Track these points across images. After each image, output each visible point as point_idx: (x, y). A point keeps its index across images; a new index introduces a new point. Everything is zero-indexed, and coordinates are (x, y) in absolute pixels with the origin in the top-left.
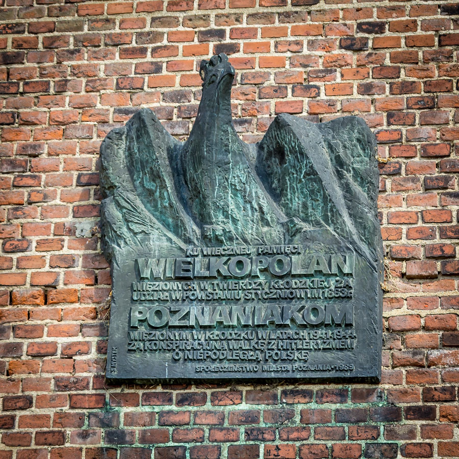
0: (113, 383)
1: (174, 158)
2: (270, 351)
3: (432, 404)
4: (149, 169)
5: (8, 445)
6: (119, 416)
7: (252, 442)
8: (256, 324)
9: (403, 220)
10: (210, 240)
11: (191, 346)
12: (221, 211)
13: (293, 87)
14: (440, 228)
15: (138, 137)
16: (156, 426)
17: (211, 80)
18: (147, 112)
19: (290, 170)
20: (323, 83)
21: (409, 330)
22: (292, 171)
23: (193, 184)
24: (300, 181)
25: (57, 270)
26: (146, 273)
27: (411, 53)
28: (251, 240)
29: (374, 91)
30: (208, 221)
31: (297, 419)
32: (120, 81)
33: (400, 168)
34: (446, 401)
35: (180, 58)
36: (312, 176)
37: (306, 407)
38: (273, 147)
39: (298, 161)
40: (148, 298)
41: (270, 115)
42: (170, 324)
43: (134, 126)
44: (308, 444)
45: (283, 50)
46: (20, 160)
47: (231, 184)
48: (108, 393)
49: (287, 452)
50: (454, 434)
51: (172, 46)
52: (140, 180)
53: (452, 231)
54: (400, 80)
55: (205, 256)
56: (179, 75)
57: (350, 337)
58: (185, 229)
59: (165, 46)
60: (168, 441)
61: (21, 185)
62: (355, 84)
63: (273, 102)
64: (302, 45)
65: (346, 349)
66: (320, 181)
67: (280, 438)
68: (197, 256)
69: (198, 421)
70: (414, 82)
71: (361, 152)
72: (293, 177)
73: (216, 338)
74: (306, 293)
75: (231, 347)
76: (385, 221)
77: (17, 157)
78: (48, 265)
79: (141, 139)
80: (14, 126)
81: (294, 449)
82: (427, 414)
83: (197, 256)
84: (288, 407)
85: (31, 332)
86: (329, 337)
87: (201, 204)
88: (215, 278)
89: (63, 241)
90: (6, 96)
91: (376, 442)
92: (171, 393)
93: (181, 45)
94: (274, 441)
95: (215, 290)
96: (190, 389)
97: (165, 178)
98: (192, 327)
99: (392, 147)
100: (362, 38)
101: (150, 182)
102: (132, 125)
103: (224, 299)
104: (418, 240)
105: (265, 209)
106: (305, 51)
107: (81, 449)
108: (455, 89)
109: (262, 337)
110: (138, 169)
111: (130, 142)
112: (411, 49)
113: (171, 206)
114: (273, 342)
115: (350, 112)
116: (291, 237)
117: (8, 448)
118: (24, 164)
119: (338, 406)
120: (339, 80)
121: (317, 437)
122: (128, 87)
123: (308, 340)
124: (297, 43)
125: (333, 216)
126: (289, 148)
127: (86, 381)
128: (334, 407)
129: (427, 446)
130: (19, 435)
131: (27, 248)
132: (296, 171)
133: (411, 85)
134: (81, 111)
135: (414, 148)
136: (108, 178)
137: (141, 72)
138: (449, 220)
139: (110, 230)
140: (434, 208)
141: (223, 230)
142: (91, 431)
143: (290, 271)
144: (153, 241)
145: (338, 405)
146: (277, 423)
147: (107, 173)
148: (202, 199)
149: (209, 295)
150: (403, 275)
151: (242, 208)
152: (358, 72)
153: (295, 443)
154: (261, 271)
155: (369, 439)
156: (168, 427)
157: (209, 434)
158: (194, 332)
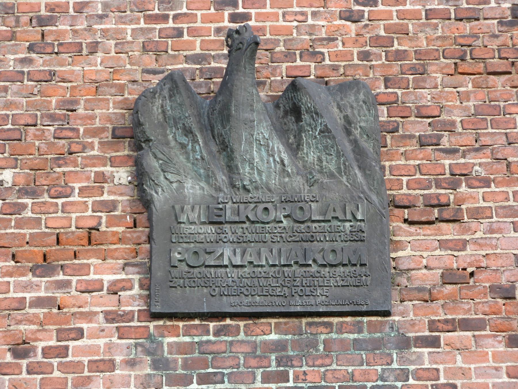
0: (156, 316)
1: (202, 115)
2: (295, 288)
3: (437, 334)
4: (181, 125)
5: (63, 373)
6: (162, 346)
7: (282, 368)
8: (282, 264)
9: (403, 173)
10: (238, 188)
11: (226, 284)
12: (247, 164)
13: (301, 53)
14: (435, 179)
15: (170, 97)
16: (196, 355)
17: (238, 47)
18: (178, 74)
19: (306, 128)
20: (327, 50)
21: (414, 270)
22: (308, 128)
23: (221, 139)
24: (316, 137)
25: (99, 214)
26: (183, 218)
27: (402, 25)
28: (275, 189)
29: (372, 57)
30: (236, 172)
31: (321, 347)
32: (146, 44)
33: (398, 127)
34: (449, 332)
35: (199, 24)
36: (327, 134)
37: (327, 337)
38: (289, 107)
39: (314, 120)
40: (186, 240)
41: (282, 78)
42: (206, 264)
43: (166, 86)
44: (331, 370)
45: (290, 19)
46: (59, 114)
47: (256, 140)
48: (152, 325)
49: (313, 377)
50: (457, 360)
51: (192, 13)
52: (173, 134)
53: (446, 183)
54: (393, 48)
55: (234, 203)
56: (198, 40)
57: (365, 275)
58: (216, 179)
59: (185, 14)
60: (208, 368)
61: (61, 136)
62: (355, 51)
63: (284, 65)
64: (307, 16)
65: (362, 286)
66: (334, 138)
67: (307, 364)
68: (227, 203)
69: (234, 350)
70: (406, 51)
71: (367, 112)
72: (309, 134)
73: (249, 276)
74: (325, 237)
75: (261, 285)
76: (387, 172)
77: (56, 111)
78: (90, 209)
79: (173, 98)
80: (51, 83)
81: (319, 374)
82: (434, 342)
83: (227, 203)
84: (312, 337)
85: (79, 270)
86: (346, 276)
87: (228, 157)
88: (244, 222)
89: (103, 187)
90: (43, 55)
91: (390, 367)
92: (208, 325)
93: (199, 13)
94: (301, 367)
95: (245, 233)
96: (225, 321)
97: (197, 134)
98: (226, 266)
99: (390, 108)
100: (359, 10)
101: (182, 136)
102: (164, 85)
103: (253, 242)
104: (417, 190)
105: (286, 162)
106: (310, 21)
107: (130, 376)
108: (441, 57)
109: (288, 275)
110: (171, 125)
111: (162, 100)
112: (401, 21)
113: (203, 159)
114: (298, 279)
115: (352, 76)
116: (310, 187)
117: (63, 376)
118: (62, 117)
119: (356, 336)
120: (340, 48)
121: (339, 363)
122: (154, 50)
123: (328, 278)
124: (303, 14)
125: (345, 168)
126: (305, 108)
127: (132, 314)
128: (352, 336)
129: (434, 371)
130: (73, 363)
131: (71, 194)
132: (312, 128)
133: (404, 53)
134: (112, 70)
135: (409, 109)
136: (145, 132)
137: (164, 37)
138: (443, 173)
139: (148, 179)
140: (429, 162)
141: (250, 181)
142: (138, 360)
143: (311, 217)
144: (188, 190)
145: (356, 335)
146: (303, 351)
147: (143, 128)
148: (230, 153)
149: (239, 238)
150: (406, 221)
151: (266, 161)
152: (357, 40)
153: (320, 368)
154: (285, 217)
155: (384, 365)
156: (207, 355)
157: (244, 361)
158: (228, 270)
